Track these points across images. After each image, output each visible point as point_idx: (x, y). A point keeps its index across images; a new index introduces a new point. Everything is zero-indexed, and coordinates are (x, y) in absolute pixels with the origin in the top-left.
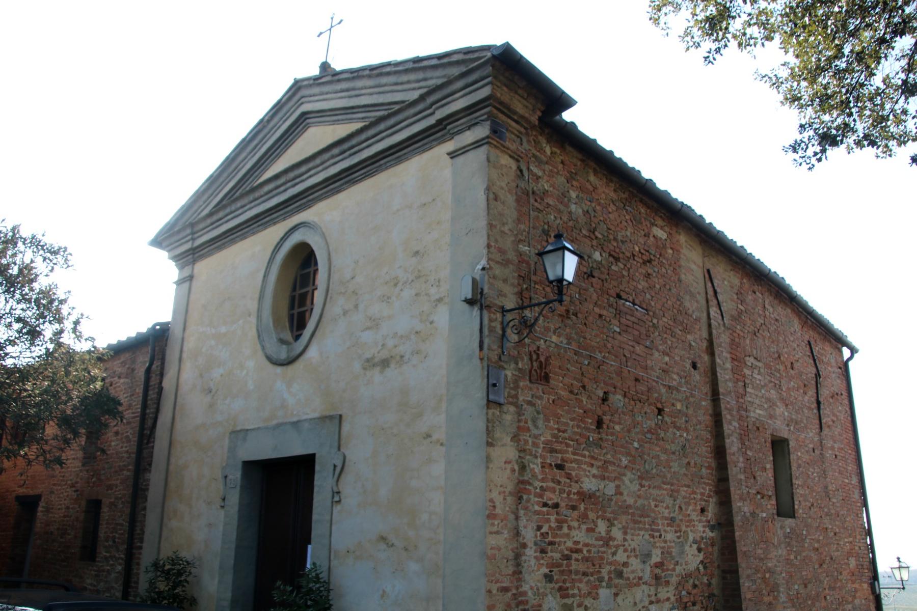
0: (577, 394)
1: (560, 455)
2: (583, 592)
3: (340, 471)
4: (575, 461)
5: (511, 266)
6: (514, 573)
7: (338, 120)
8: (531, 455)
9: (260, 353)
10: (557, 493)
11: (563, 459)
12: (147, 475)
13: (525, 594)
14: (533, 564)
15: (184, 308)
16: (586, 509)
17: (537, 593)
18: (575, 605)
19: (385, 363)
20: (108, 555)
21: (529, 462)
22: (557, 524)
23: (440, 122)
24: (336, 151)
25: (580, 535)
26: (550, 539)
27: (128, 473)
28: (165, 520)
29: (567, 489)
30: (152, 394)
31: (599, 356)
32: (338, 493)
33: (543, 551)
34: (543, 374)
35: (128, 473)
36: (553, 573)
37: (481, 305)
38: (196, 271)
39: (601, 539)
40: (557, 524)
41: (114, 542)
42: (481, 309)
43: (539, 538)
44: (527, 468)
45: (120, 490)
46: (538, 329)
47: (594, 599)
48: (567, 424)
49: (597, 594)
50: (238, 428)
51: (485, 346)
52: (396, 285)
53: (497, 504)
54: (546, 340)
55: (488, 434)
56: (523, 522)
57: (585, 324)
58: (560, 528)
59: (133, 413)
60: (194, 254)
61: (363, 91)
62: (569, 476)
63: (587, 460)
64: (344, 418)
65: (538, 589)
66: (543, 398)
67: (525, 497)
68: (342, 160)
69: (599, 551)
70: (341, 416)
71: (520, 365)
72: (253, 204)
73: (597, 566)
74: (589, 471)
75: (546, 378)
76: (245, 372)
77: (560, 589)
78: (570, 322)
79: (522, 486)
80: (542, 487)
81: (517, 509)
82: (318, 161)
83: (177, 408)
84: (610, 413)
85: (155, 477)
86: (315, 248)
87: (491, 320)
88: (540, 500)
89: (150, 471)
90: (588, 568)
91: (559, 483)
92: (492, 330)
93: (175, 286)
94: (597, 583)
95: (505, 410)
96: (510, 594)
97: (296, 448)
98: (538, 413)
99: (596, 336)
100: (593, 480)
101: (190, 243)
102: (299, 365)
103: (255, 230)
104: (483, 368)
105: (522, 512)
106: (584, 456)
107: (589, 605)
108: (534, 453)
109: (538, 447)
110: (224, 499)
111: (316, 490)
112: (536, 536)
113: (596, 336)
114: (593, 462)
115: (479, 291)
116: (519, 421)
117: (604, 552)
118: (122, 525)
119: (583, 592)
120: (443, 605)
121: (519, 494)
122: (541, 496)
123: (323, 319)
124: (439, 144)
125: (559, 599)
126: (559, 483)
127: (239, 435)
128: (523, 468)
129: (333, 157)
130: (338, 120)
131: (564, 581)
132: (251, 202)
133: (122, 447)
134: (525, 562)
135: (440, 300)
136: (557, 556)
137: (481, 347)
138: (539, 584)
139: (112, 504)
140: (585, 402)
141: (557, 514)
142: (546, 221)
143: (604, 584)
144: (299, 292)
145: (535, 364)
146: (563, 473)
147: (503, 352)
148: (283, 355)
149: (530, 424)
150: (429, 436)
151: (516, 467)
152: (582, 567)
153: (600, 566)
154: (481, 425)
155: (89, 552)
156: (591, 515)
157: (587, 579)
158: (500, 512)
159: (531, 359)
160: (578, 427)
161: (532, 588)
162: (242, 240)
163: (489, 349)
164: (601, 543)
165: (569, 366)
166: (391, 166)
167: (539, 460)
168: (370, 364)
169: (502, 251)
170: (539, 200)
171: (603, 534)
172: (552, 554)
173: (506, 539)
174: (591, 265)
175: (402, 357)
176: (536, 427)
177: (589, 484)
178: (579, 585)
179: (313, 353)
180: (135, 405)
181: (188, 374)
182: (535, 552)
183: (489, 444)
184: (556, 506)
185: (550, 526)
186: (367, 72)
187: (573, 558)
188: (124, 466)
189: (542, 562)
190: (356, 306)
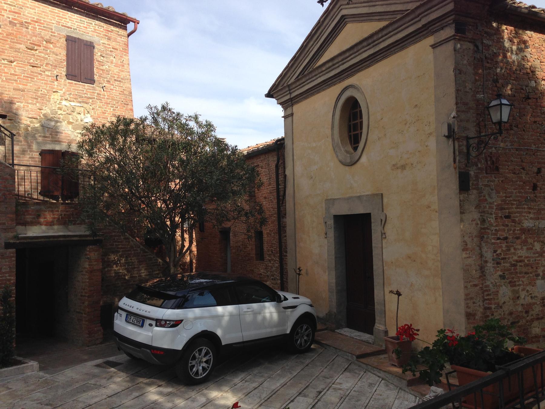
0: (518, 174)
1: (507, 211)
2: (525, 283)
3: (384, 222)
4: (517, 212)
5: (471, 111)
6: (480, 277)
7: (364, 20)
8: (488, 214)
10: (506, 231)
11: (509, 213)
12: (284, 220)
13: (488, 286)
14: (492, 271)
15: (289, 126)
16: (526, 238)
17: (495, 285)
18: (520, 290)
19: (403, 167)
20: (270, 258)
21: (487, 217)
22: (506, 248)
23: (424, 26)
24: (365, 44)
25: (523, 253)
26: (502, 256)
27: (274, 219)
28: (297, 243)
29: (513, 229)
30: (281, 178)
31: (533, 147)
32: (385, 233)
33: (498, 263)
34: (494, 167)
35: (274, 219)
36: (505, 274)
37: (454, 139)
38: (294, 110)
39: (537, 253)
40: (506, 248)
41: (272, 252)
42: (454, 141)
43: (495, 257)
44: (486, 221)
45: (271, 227)
46: (491, 142)
47: (533, 286)
48: (512, 193)
49: (535, 283)
50: (329, 198)
51: (457, 161)
52: (406, 124)
53: (468, 243)
54: (496, 147)
55: (460, 208)
56: (485, 249)
57: (524, 130)
58: (509, 250)
59: (272, 188)
60: (292, 101)
62: (514, 221)
63: (526, 210)
64: (384, 195)
65: (496, 283)
66: (495, 180)
67: (485, 236)
68: (369, 49)
69: (535, 260)
70: (382, 194)
71: (479, 165)
72: (321, 74)
73: (535, 268)
74: (528, 216)
75: (497, 169)
76: (328, 169)
77: (510, 282)
78: (512, 132)
79: (483, 231)
80: (496, 229)
81: (481, 244)
82: (355, 50)
83: (295, 186)
84: (543, 180)
85: (289, 220)
86: (359, 101)
87: (459, 146)
88: (496, 236)
89: (286, 218)
90: (528, 269)
91: (507, 226)
92: (460, 152)
93: (283, 119)
94: (535, 277)
95: (471, 193)
96: (478, 287)
97: (360, 210)
98: (492, 190)
99: (532, 135)
100: (531, 221)
101: (289, 95)
102: (358, 165)
103: (324, 88)
104: (456, 173)
105: (484, 244)
106: (525, 208)
107: (529, 290)
108: (490, 212)
109: (493, 209)
110: (326, 234)
111: (373, 231)
112: (493, 256)
113: (532, 135)
114: (530, 211)
115: (452, 130)
116: (480, 197)
117: (540, 260)
118: (275, 244)
119: (525, 283)
120: (443, 293)
121: (481, 236)
122: (496, 234)
123: (368, 142)
124: (425, 38)
125: (509, 288)
126: (507, 226)
127: (330, 202)
128: (483, 221)
129: (363, 47)
130: (364, 20)
131: (513, 278)
132: (320, 73)
133: (269, 205)
134: (487, 270)
135: (430, 134)
136: (508, 265)
137: (455, 161)
138: (496, 281)
139: (268, 234)
140: (524, 178)
141: (507, 242)
142: (495, 74)
143: (540, 277)
144: (352, 123)
145: (489, 162)
146: (510, 220)
147: (468, 162)
148: (348, 160)
149: (487, 197)
150: (429, 207)
151: (479, 222)
152: (524, 270)
153: (537, 268)
154: (457, 203)
155: (260, 256)
156: (530, 241)
157: (528, 275)
158: (470, 247)
159: (486, 161)
160: (520, 192)
161: (492, 283)
162: (317, 93)
163: (459, 163)
164: (537, 255)
165: (512, 159)
166: (398, 52)
167: (494, 216)
168: (395, 167)
169: (466, 104)
170: (490, 61)
171: (539, 250)
172: (504, 264)
173: (474, 260)
174: (528, 91)
175: (412, 164)
176: (491, 198)
177: (527, 224)
178: (523, 279)
179: (364, 159)
180: (273, 183)
181: (299, 169)
182: (493, 264)
183: (462, 213)
184: (506, 238)
185: (502, 250)
187: (518, 265)
188: (272, 214)
189: (498, 269)
190: (385, 135)
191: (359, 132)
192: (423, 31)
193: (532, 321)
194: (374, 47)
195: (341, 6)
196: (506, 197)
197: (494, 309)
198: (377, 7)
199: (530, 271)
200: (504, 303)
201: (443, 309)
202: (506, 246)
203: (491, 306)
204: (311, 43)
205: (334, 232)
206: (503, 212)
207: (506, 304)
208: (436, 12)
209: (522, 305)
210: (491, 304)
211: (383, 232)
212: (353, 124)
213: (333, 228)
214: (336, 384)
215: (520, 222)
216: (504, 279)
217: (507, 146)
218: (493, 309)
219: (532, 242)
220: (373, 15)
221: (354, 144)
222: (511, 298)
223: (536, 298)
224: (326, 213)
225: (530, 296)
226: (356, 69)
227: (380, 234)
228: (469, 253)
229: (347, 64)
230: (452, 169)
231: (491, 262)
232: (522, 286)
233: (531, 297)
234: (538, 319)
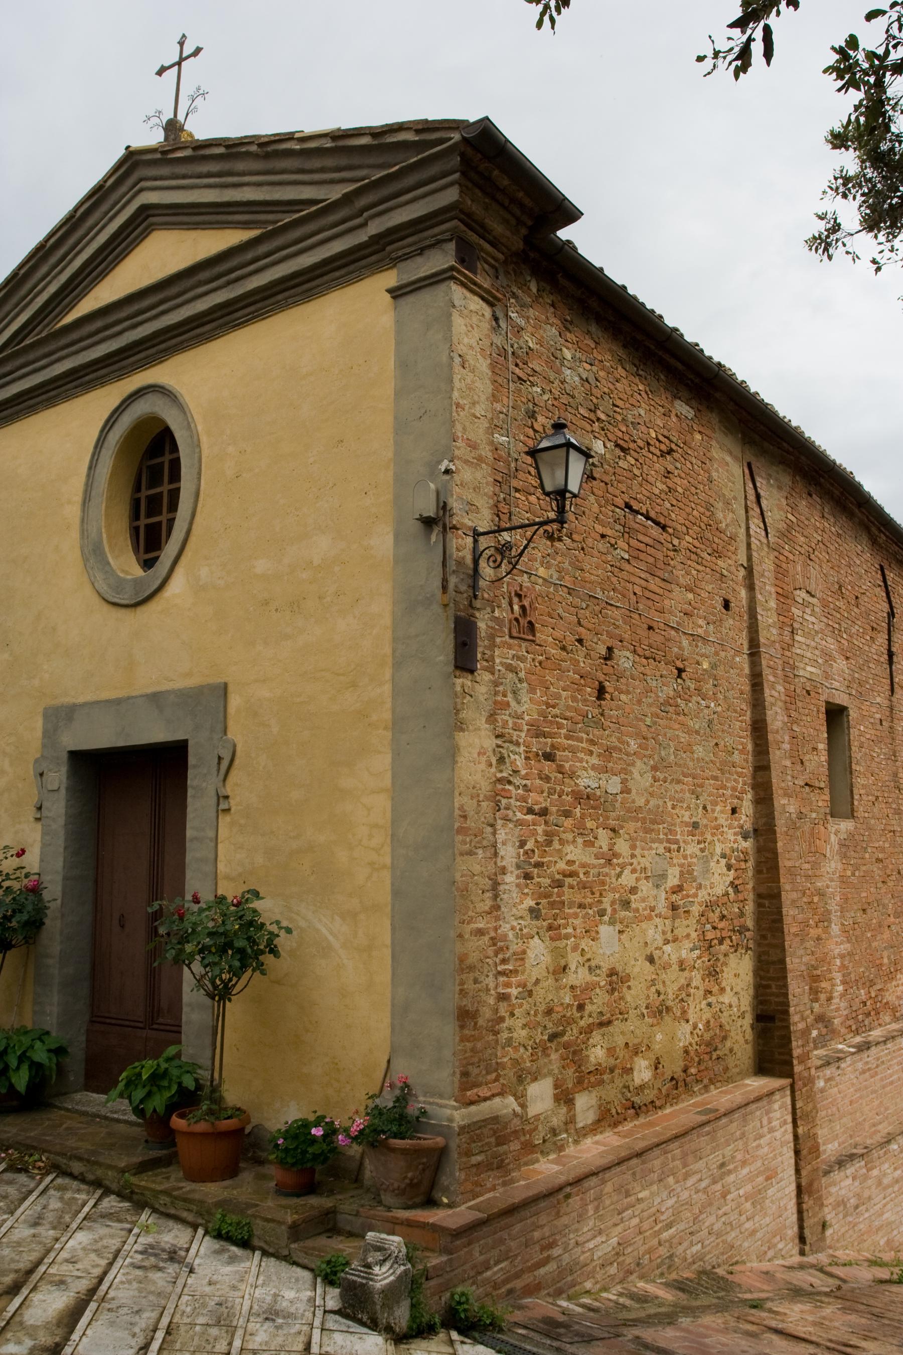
1: (549, 740)
8: (511, 742)
9: (88, 590)
11: (553, 746)
16: (583, 817)
18: (569, 948)
23: (376, 239)
25: (576, 853)
33: (527, 876)
36: (540, 906)
43: (522, 858)
44: (507, 760)
47: (593, 940)
49: (597, 932)
51: (451, 586)
61: (247, 179)
63: (584, 745)
64: (231, 688)
70: (226, 685)
73: (597, 895)
88: (524, 804)
106: (580, 740)
108: (515, 738)
110: (40, 808)
111: (190, 792)
112: (519, 854)
123: (193, 539)
126: (547, 779)
137: (445, 588)
141: (546, 823)
147: (475, 597)
149: (510, 698)
153: (601, 894)
156: (590, 824)
157: (584, 912)
159: (511, 605)
160: (574, 699)
171: (605, 848)
177: (586, 780)
179: (177, 585)
182: (518, 877)
184: (544, 812)
185: (536, 841)
186: (221, 150)
187: (567, 884)
191: (163, 518)
192: (371, 255)
193: (588, 1031)
194: (231, 286)
195: (141, 180)
196: (548, 705)
197: (517, 998)
198: (245, 188)
199: (589, 900)
200: (537, 981)
201: (393, 1005)
202: (546, 833)
203: (509, 990)
204: (44, 269)
205: (68, 801)
206: (540, 743)
207: (541, 985)
208: (408, 207)
209: (572, 987)
210: (508, 985)
211: (222, 792)
212: (147, 497)
213: (63, 791)
214: (118, 1289)
215: (572, 775)
216: (537, 918)
217: (551, 577)
218: (513, 998)
219: (594, 827)
220: (231, 209)
221: (147, 551)
222: (551, 970)
223: (598, 971)
224: (44, 746)
225: (587, 965)
226: (174, 341)
227: (215, 799)
228: (471, 841)
229: (146, 325)
230: (437, 608)
231: (512, 872)
232: (573, 939)
233: (590, 968)
234: (601, 1025)
